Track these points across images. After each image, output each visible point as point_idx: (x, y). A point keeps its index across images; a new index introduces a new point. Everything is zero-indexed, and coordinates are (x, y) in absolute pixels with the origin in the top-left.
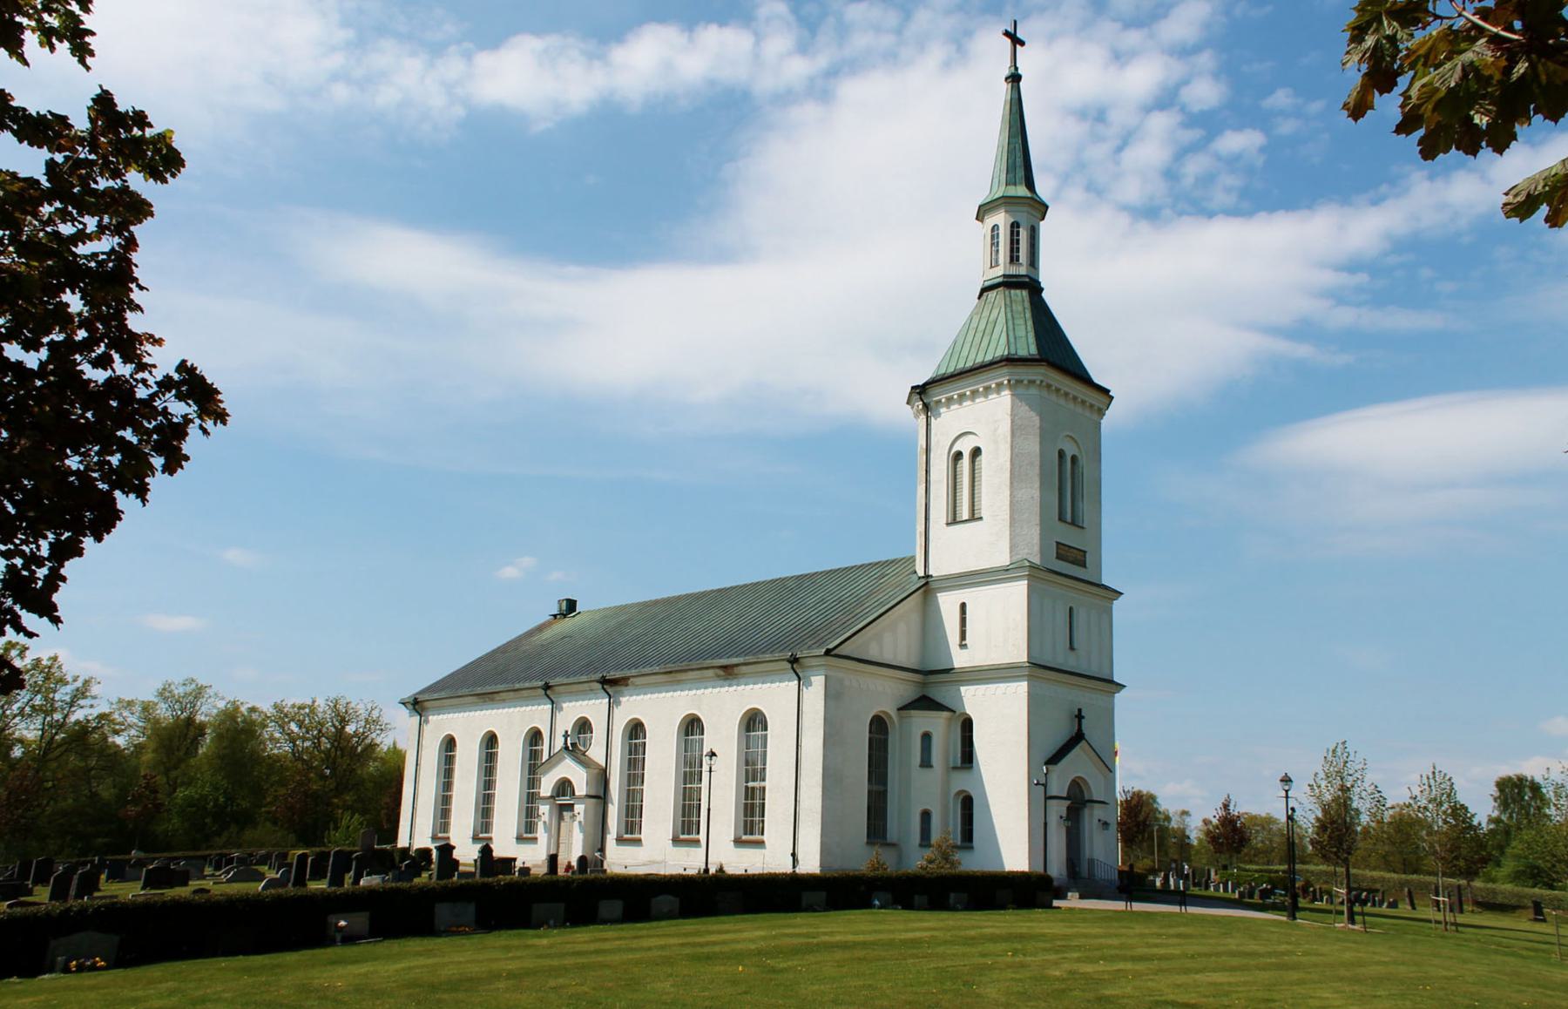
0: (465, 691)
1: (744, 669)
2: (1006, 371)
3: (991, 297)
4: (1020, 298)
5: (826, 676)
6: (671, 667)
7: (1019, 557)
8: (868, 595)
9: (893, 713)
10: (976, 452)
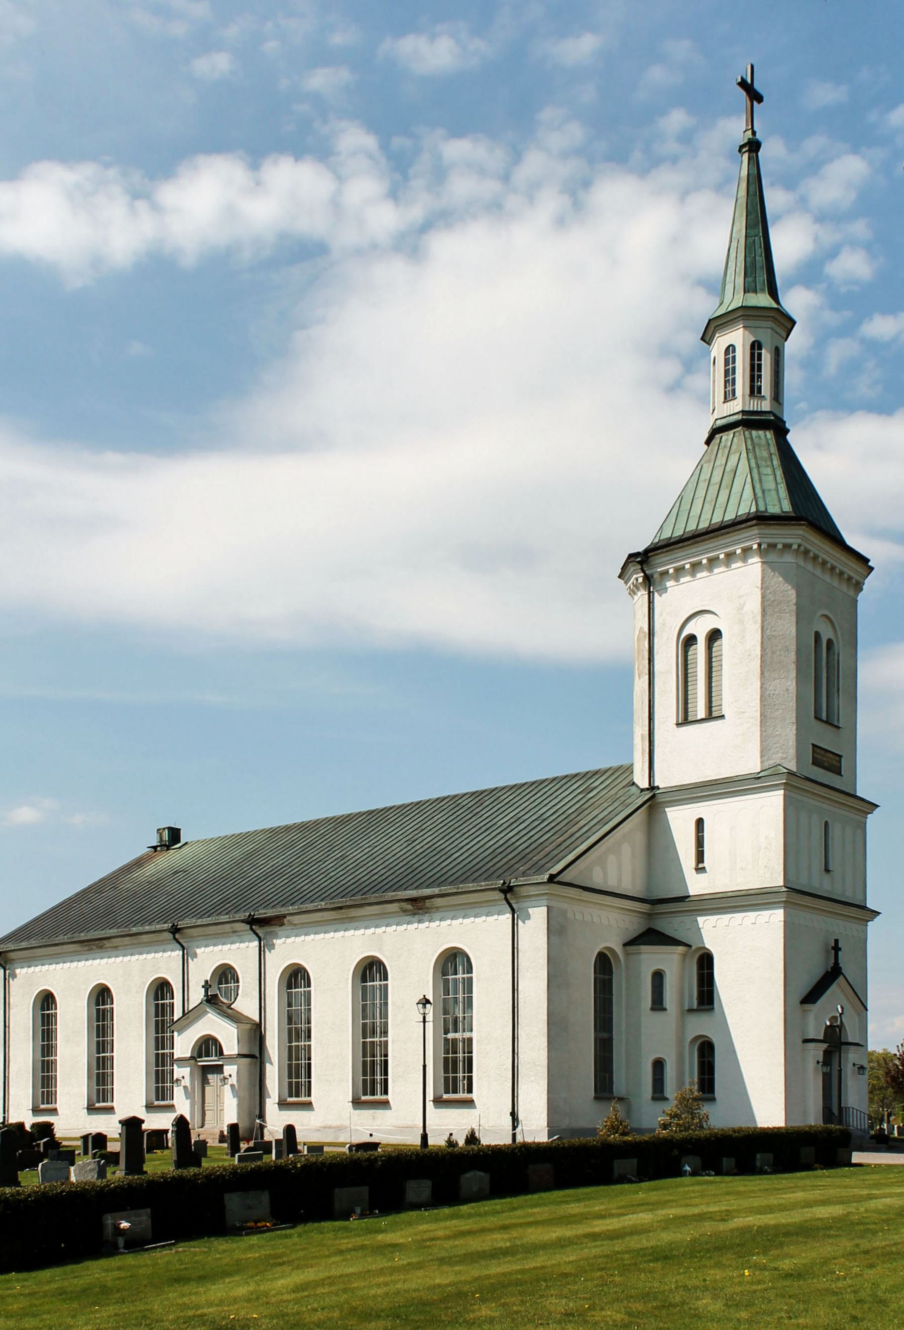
0: (61, 938)
1: (439, 902)
2: (756, 532)
3: (727, 440)
4: (763, 442)
5: (548, 907)
6: (339, 901)
7: (771, 763)
8: (580, 811)
9: (619, 950)
10: (714, 635)
